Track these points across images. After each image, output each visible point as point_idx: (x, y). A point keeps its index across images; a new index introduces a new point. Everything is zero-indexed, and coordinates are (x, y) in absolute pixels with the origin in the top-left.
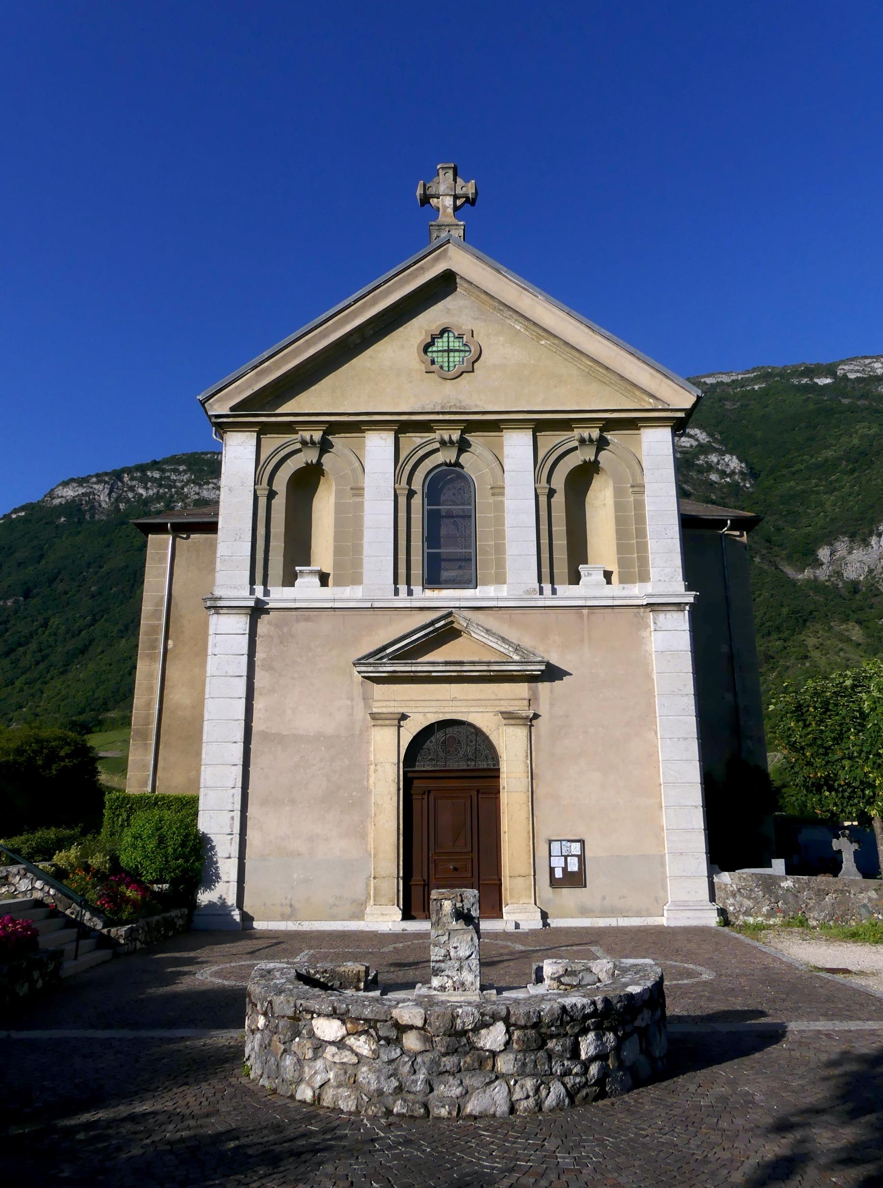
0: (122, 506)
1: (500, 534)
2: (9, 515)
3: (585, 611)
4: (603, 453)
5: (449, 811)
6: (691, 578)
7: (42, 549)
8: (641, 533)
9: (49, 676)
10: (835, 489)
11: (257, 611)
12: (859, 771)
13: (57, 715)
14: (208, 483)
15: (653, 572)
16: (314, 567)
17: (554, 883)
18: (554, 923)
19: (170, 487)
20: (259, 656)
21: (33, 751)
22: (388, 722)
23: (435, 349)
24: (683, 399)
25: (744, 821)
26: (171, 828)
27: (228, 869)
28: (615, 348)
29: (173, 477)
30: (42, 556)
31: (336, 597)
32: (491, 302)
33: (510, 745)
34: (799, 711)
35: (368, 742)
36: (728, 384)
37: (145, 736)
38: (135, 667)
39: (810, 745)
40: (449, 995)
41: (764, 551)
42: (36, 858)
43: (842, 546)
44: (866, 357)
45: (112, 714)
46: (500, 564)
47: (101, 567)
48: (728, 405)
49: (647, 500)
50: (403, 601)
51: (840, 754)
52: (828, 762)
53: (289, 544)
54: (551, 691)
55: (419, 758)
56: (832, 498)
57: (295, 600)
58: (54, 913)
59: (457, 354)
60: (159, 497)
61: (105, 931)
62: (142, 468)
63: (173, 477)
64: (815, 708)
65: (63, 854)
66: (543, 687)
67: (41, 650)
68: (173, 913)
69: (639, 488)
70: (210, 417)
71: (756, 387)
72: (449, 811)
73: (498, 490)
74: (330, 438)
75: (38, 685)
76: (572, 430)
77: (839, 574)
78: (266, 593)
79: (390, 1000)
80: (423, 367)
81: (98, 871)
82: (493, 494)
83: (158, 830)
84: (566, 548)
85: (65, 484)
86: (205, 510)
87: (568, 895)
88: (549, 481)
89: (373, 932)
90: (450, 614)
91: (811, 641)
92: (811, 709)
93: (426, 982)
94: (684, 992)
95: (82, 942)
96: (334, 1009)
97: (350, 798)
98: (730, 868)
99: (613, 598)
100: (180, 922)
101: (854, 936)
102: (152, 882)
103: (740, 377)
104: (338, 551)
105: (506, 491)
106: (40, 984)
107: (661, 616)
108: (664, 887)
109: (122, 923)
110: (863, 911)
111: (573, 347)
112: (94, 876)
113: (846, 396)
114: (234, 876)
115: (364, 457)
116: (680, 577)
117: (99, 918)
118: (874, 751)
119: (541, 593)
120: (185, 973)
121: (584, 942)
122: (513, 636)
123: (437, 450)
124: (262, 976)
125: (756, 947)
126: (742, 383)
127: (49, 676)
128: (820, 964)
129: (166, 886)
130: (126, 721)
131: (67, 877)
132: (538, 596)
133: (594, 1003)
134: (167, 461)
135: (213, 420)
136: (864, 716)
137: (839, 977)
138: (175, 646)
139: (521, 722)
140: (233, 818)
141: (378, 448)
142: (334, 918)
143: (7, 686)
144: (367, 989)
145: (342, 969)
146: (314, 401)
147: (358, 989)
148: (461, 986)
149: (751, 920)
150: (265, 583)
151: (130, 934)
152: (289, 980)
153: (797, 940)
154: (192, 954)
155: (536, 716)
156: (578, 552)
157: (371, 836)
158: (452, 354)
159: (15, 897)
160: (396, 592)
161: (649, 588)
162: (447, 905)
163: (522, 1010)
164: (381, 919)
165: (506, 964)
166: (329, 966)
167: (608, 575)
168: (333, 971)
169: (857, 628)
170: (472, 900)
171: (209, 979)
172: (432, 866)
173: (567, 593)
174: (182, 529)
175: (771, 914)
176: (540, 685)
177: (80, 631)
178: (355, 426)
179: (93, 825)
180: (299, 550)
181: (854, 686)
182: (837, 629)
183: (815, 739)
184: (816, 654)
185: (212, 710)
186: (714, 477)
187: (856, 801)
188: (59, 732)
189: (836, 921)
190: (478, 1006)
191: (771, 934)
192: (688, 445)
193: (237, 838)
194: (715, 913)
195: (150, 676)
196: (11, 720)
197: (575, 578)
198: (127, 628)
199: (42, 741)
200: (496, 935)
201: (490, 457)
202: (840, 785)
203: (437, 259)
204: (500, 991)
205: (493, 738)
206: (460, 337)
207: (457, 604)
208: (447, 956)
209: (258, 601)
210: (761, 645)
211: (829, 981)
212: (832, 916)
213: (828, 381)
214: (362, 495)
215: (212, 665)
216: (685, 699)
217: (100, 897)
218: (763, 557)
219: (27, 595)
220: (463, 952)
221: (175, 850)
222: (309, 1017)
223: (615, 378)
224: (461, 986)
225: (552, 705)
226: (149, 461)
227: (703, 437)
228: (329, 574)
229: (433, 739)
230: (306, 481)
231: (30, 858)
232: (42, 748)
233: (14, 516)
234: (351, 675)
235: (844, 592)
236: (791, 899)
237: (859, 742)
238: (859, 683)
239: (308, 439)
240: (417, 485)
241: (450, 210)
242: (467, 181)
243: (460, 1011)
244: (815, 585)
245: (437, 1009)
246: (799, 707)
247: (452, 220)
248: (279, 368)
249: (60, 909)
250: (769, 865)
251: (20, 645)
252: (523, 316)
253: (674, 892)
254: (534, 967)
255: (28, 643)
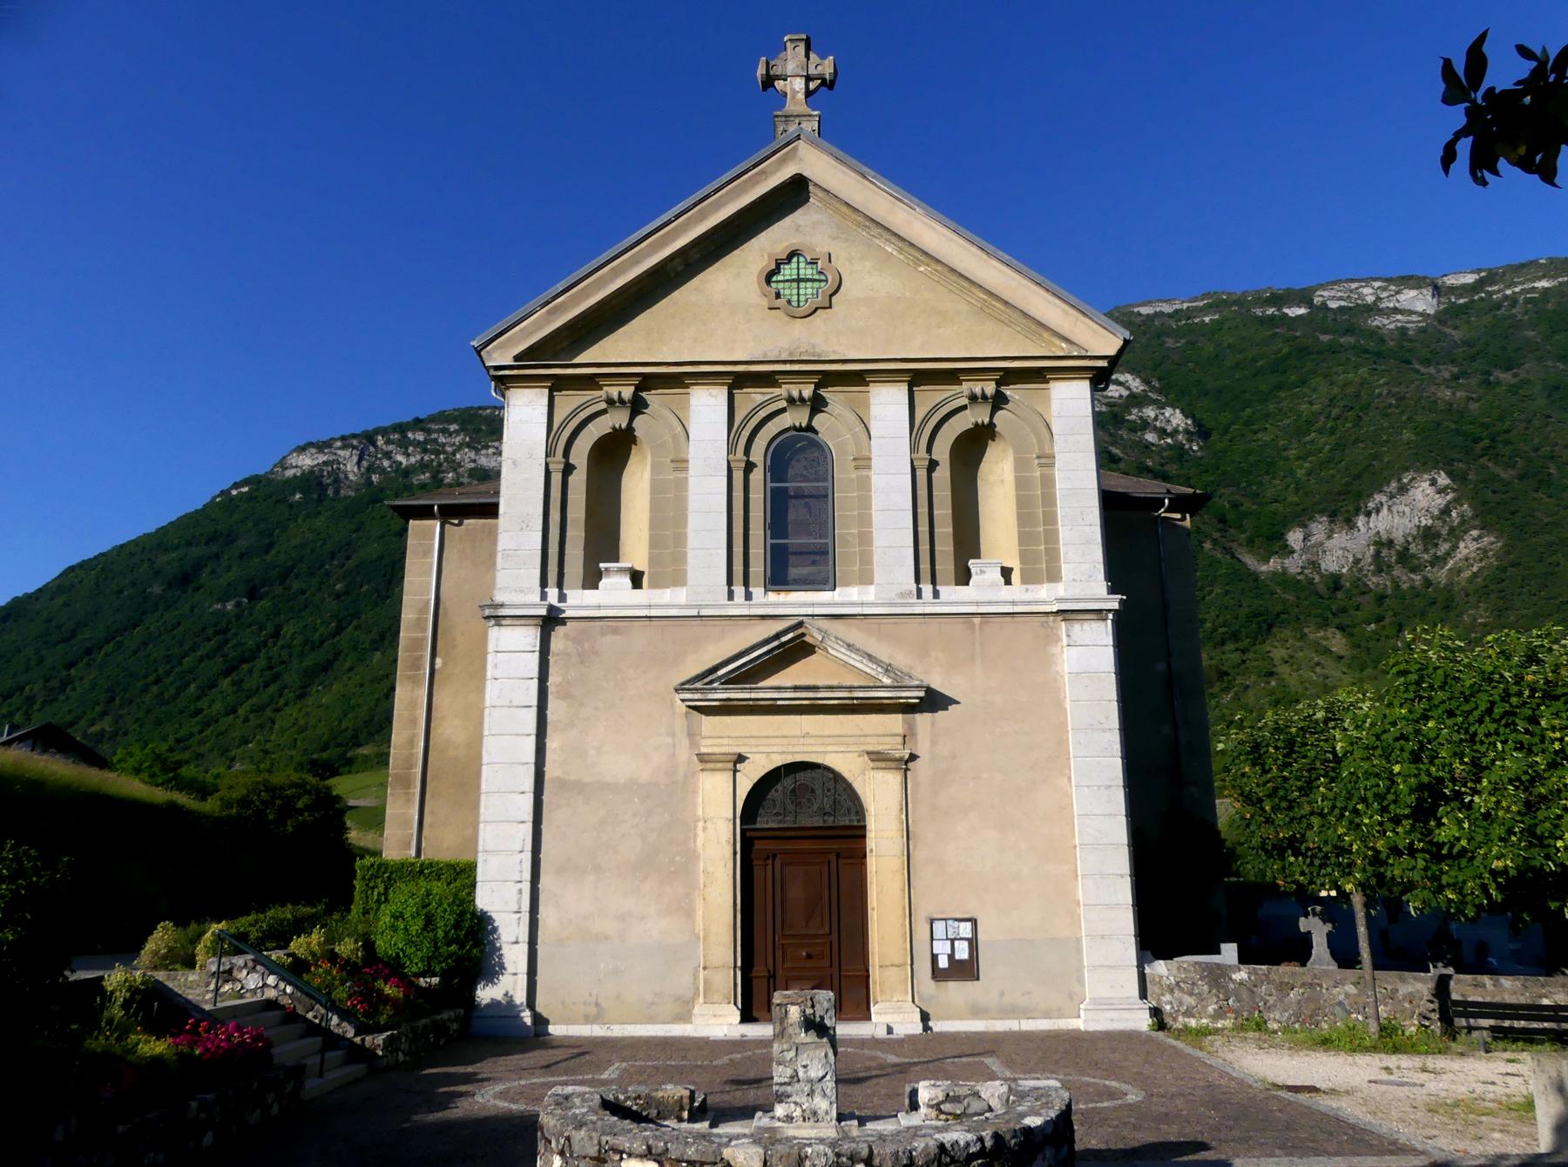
0: (375, 478)
1: (865, 519)
2: (228, 491)
3: (977, 620)
4: (1000, 413)
5: (800, 882)
6: (1116, 575)
7: (271, 535)
8: (1050, 518)
9: (282, 702)
10: (1310, 454)
11: (551, 621)
12: (1330, 832)
13: (293, 753)
14: (487, 447)
15: (1065, 569)
16: (624, 564)
17: (938, 974)
18: (937, 1026)
19: (437, 453)
20: (553, 680)
21: (263, 802)
22: (720, 765)
23: (780, 278)
24: (1104, 342)
25: (1188, 891)
26: (440, 904)
27: (514, 957)
28: (1016, 276)
29: (442, 439)
30: (272, 544)
31: (653, 602)
32: (854, 216)
33: (879, 796)
34: (1256, 752)
35: (695, 792)
36: (1170, 316)
37: (406, 783)
38: (393, 689)
39: (1269, 796)
40: (799, 1127)
41: (1217, 535)
42: (269, 945)
43: (1319, 528)
44: (1352, 281)
45: (366, 750)
46: (866, 559)
47: (348, 558)
48: (1170, 342)
49: (1058, 475)
50: (739, 607)
51: (1307, 808)
52: (1293, 819)
53: (590, 530)
54: (933, 725)
55: (761, 811)
56: (1307, 465)
57: (599, 607)
58: (291, 1017)
59: (809, 284)
60: (423, 466)
61: (358, 1040)
62: (401, 428)
63: (442, 439)
64: (1277, 748)
65: (302, 939)
66: (922, 719)
67: (271, 668)
68: (445, 1016)
69: (1047, 460)
70: (488, 369)
71: (1207, 319)
72: (800, 882)
73: (863, 462)
74: (644, 394)
75: (268, 713)
76: (959, 383)
77: (1315, 565)
78: (562, 598)
79: (720, 1136)
80: (765, 303)
81: (348, 961)
82: (857, 468)
83: (424, 907)
84: (951, 540)
85: (301, 449)
86: (483, 488)
87: (956, 991)
88: (929, 450)
89: (702, 1039)
90: (800, 624)
91: (1279, 653)
92: (1272, 750)
93: (768, 1109)
94: (1101, 1118)
95: (329, 1055)
96: (649, 1148)
97: (670, 864)
98: (1167, 955)
99: (1014, 603)
100: (455, 1026)
101: (1325, 1043)
102: (418, 975)
103: (1185, 306)
104: (655, 542)
105: (873, 463)
106: (275, 1110)
107: (1077, 627)
108: (1081, 981)
109: (381, 1030)
110: (1338, 1010)
111: (961, 275)
112: (342, 968)
113: (1325, 332)
114: (523, 966)
115: (688, 418)
116: (1101, 576)
117: (350, 1023)
118: (1350, 807)
119: (919, 595)
120: (462, 1094)
121: (972, 1054)
122: (883, 652)
123: (783, 410)
124: (558, 1104)
125: (1198, 1059)
126: (1189, 314)
127: (282, 702)
128: (1280, 1081)
129: (435, 980)
130: (383, 760)
131: (308, 971)
132: (915, 600)
133: (981, 1139)
134: (433, 419)
135: (493, 372)
136: (1338, 760)
137: (1303, 1098)
138: (444, 664)
139: (893, 765)
140: (520, 891)
141: (707, 408)
142: (652, 1020)
143: (227, 714)
144: (692, 1119)
145: (660, 1094)
146: (622, 347)
147: (680, 1120)
148: (813, 1116)
149: (1193, 1023)
150: (560, 585)
151: (389, 1042)
152: (591, 1110)
153: (1251, 1048)
154: (470, 1069)
155: (913, 757)
156: (968, 543)
157: (700, 913)
158: (802, 285)
159: (242, 997)
160: (731, 596)
161: (1060, 590)
162: (794, 1012)
163: (889, 1149)
164: (713, 1021)
165: (874, 1081)
166: (643, 1090)
167: (1006, 573)
168: (648, 1096)
169: (1339, 635)
170: (826, 1005)
171: (493, 1102)
172: (779, 954)
173: (954, 597)
174: (452, 513)
175: (1220, 1014)
176: (918, 716)
177: (323, 642)
178: (677, 380)
179: (341, 899)
180: (604, 541)
181: (1326, 721)
182: (1312, 636)
183: (1275, 789)
184: (1284, 670)
185: (492, 750)
186: (1150, 437)
187: (1329, 870)
188: (295, 777)
189: (1303, 1023)
190: (833, 1144)
191: (1219, 1041)
192: (1116, 395)
193: (526, 917)
194: (1147, 1014)
195: (413, 704)
196: (233, 759)
197: (963, 577)
198: (382, 637)
199: (275, 788)
200: (862, 1043)
201: (852, 418)
202: (1308, 849)
203: (783, 161)
204: (862, 1121)
205: (858, 786)
206: (813, 262)
207: (809, 611)
208: (795, 1077)
209: (551, 608)
210: (1207, 658)
211: (1290, 1103)
212: (1297, 1015)
213: (1302, 311)
214: (686, 469)
215: (492, 693)
216: (1108, 734)
217: (350, 996)
218: (1215, 542)
219: (253, 594)
220: (815, 1072)
221: (446, 933)
222: (617, 1157)
223: (1015, 315)
224: (813, 1116)
225: (933, 743)
226: (410, 419)
227: (1136, 384)
228: (642, 573)
229: (779, 787)
230: (613, 453)
231: (258, 946)
232: (274, 798)
233: (234, 492)
234: (672, 705)
235: (1322, 589)
236: (1245, 995)
237: (1330, 795)
238: (1333, 717)
239: (616, 397)
240: (757, 455)
241: (801, 96)
242: (823, 57)
243: (809, 1150)
244: (1282, 578)
245: (779, 1147)
246: (1256, 747)
247: (803, 108)
248: (578, 304)
249: (300, 1011)
250: (1218, 952)
251: (244, 660)
252: (896, 235)
253: (1093, 987)
254: (908, 1089)
255: (254, 658)
